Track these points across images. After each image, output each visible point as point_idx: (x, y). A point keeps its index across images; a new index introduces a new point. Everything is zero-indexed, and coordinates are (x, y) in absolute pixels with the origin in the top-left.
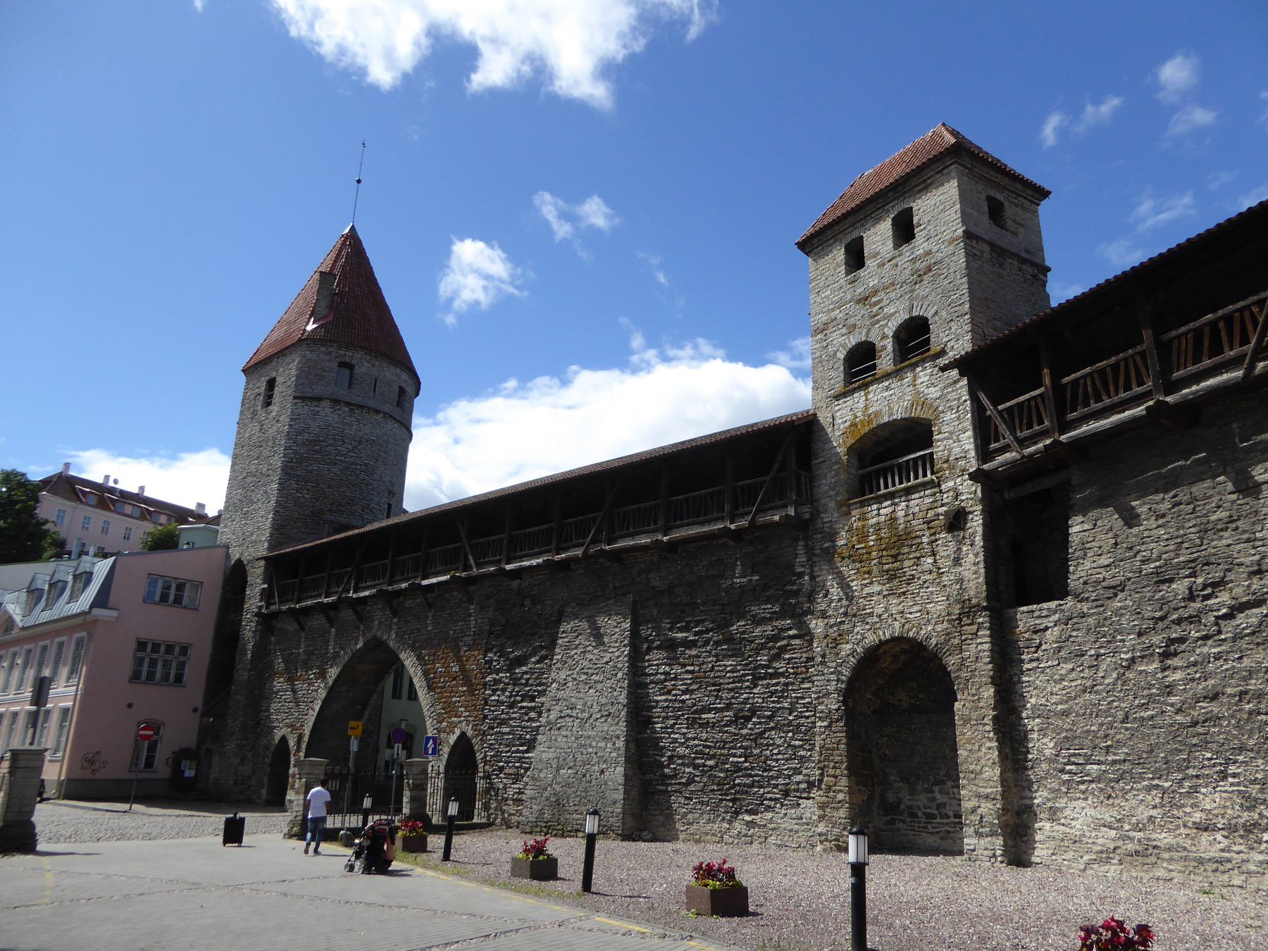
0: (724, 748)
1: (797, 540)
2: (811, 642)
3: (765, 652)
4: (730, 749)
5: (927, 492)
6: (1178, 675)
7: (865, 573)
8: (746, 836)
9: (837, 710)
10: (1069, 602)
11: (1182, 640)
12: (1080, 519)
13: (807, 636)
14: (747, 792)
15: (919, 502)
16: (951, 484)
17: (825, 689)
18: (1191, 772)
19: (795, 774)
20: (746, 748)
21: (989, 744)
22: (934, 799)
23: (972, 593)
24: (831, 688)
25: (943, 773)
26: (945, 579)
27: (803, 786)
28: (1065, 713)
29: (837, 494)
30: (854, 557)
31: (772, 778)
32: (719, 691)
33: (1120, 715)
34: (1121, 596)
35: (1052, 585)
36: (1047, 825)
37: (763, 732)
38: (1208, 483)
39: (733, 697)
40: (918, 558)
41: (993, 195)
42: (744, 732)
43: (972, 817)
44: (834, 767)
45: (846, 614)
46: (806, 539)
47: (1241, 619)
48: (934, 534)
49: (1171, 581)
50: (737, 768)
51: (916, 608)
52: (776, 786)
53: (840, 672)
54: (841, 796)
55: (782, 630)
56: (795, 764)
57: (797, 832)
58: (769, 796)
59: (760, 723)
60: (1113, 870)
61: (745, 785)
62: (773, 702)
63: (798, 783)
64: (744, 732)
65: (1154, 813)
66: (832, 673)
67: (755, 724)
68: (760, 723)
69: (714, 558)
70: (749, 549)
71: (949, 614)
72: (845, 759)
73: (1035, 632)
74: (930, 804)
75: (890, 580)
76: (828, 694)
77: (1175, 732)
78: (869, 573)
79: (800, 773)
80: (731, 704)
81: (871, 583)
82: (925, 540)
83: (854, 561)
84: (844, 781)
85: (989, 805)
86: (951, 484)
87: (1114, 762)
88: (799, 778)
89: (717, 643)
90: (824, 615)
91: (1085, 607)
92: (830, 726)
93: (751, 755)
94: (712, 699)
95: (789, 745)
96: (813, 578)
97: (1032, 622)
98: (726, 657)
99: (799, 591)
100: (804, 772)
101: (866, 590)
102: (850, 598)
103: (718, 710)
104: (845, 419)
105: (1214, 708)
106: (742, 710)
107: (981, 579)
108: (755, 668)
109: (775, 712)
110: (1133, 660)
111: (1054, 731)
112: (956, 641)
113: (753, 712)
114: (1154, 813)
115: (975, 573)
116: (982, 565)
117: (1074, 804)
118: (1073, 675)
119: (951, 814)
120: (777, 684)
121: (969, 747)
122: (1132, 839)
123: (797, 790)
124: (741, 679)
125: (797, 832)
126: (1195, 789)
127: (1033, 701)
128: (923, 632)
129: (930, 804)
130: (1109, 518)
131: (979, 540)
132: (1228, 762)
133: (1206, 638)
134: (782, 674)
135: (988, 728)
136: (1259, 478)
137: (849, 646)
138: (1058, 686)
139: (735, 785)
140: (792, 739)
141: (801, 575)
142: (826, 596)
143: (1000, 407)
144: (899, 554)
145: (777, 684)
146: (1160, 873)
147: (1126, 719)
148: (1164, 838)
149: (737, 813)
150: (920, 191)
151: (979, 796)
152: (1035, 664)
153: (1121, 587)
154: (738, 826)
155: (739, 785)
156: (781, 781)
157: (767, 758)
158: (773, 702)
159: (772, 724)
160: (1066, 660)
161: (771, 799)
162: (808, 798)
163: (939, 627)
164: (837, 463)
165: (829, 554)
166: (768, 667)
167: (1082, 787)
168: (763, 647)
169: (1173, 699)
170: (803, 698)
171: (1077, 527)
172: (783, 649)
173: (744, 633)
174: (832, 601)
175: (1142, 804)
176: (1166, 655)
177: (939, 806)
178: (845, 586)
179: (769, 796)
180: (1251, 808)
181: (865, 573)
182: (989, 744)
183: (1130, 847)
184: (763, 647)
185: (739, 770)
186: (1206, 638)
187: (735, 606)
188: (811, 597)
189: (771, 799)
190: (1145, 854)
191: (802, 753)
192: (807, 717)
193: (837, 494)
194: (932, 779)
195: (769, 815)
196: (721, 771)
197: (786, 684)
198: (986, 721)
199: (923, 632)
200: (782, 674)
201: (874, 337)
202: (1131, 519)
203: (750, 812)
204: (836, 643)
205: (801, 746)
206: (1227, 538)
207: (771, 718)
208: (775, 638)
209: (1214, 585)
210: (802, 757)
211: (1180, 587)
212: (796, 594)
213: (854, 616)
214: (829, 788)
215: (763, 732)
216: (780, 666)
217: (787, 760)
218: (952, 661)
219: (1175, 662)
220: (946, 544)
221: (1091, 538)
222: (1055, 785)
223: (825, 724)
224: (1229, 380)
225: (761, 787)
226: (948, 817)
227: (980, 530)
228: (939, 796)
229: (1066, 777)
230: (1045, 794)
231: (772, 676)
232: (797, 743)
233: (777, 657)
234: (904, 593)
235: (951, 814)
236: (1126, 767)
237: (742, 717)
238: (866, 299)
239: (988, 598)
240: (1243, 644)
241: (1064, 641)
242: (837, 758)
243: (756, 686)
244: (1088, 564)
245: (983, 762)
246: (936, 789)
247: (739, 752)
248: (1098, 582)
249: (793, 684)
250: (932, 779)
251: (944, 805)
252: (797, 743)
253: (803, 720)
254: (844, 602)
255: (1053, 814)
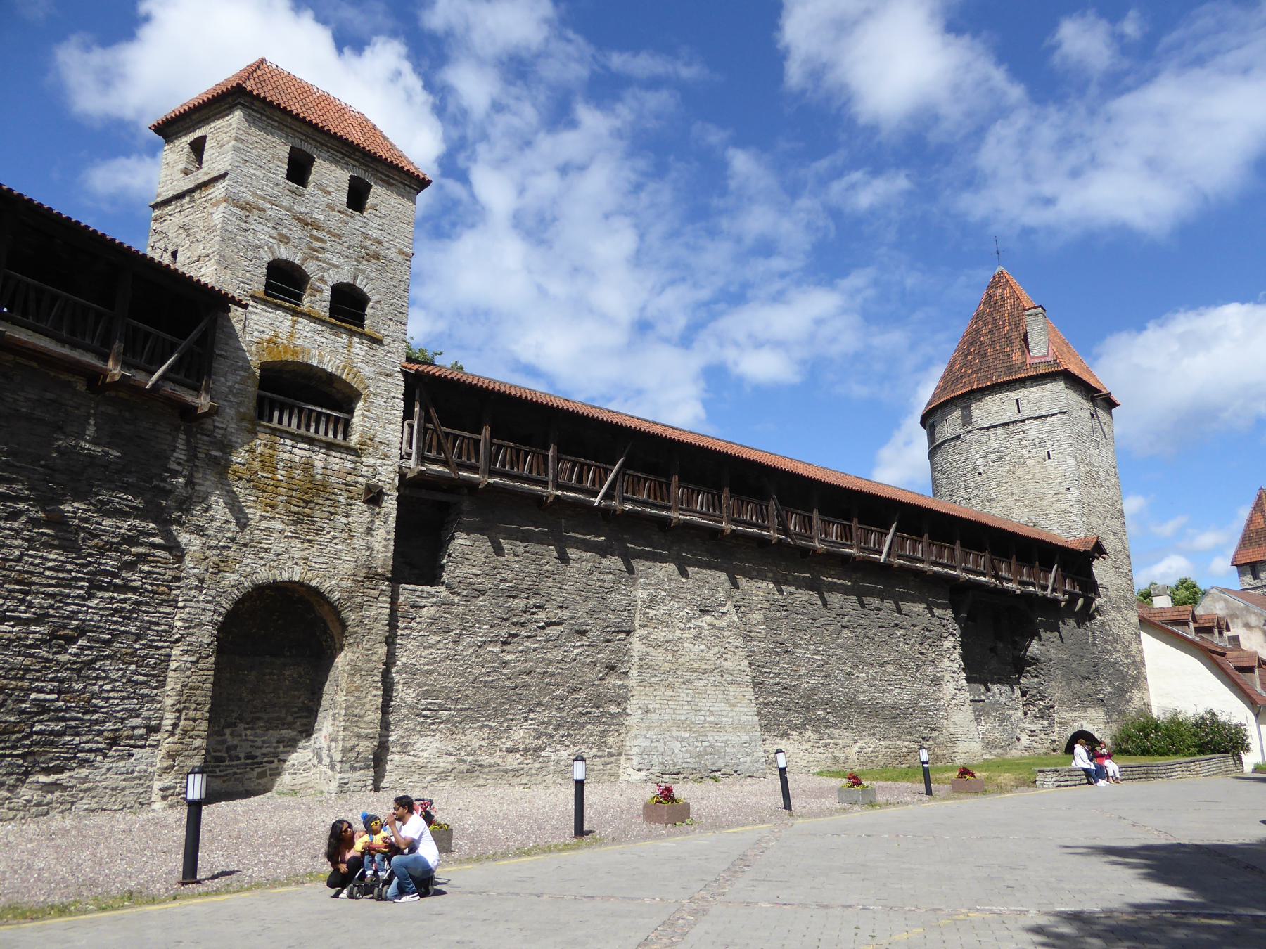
0: (22, 678)
1: (177, 429)
2: (180, 559)
3: (115, 555)
4: (33, 680)
5: (349, 457)
6: (510, 657)
7: (268, 505)
8: (39, 805)
9: (209, 645)
10: (442, 590)
11: (515, 636)
12: (464, 535)
13: (177, 552)
14: (52, 743)
15: (336, 461)
16: (372, 461)
17: (194, 618)
18: (510, 717)
19: (130, 716)
20: (61, 681)
21: (374, 692)
22: (224, 742)
23: (380, 563)
24: (206, 618)
25: (235, 715)
26: (356, 543)
27: (142, 731)
28: (430, 672)
29: (240, 404)
30: (255, 484)
31: (97, 722)
32: (27, 593)
33: (471, 678)
34: (481, 598)
35: (431, 576)
36: (397, 757)
37: (94, 661)
38: (544, 547)
39: (52, 607)
40: (332, 514)
41: (298, 146)
42: (64, 658)
43: (350, 755)
44: (196, 710)
45: (233, 540)
46: (188, 433)
47: (548, 630)
48: (351, 498)
49: (514, 597)
50: (42, 708)
51: (321, 560)
52: (100, 733)
53: (218, 604)
54: (198, 742)
55: (141, 533)
56: (133, 704)
57: (123, 790)
58: (88, 746)
59: (90, 648)
60: (448, 784)
61: (52, 733)
62: (116, 623)
63: (133, 728)
64: (64, 658)
65: (483, 743)
66: (208, 602)
67: (82, 648)
68: (90, 648)
69: (50, 396)
70: (110, 410)
71: (354, 575)
72: (208, 700)
73: (412, 607)
74: (219, 747)
75: (296, 523)
76: (201, 624)
77: (504, 692)
78: (273, 507)
79: (138, 716)
80: (47, 615)
81: (273, 518)
82: (342, 499)
83: (254, 487)
84: (204, 725)
85: (368, 743)
86: (372, 461)
87: (461, 709)
88: (136, 722)
89: (35, 522)
90: (200, 531)
91: (456, 599)
92: (197, 662)
93: (69, 690)
94: (11, 604)
95: (129, 681)
96: (190, 482)
97: (413, 599)
98: (49, 546)
99: (170, 492)
100: (145, 714)
101: (265, 524)
102: (243, 523)
103: (19, 621)
104: (261, 330)
105: (528, 678)
106: (64, 627)
107: (390, 554)
108: (95, 574)
109: (116, 635)
110: (485, 642)
111: (418, 685)
112: (359, 600)
113: (81, 631)
114: (483, 743)
115: (385, 547)
116: (392, 543)
117: (423, 739)
118: (440, 645)
119: (242, 755)
120: (125, 600)
121: (357, 694)
122: (465, 761)
123: (130, 738)
124: (69, 583)
125: (123, 790)
126: (509, 728)
127: (404, 660)
128: (327, 584)
129: (219, 747)
130: (484, 544)
131: (392, 520)
132: (531, 711)
133: (529, 637)
134: (134, 590)
135: (376, 679)
136: (572, 556)
137: (234, 577)
138: (426, 652)
139: (32, 734)
140: (134, 673)
141: (175, 474)
142: (206, 511)
143: (495, 441)
144: (312, 502)
145: (125, 600)
146: (481, 782)
147: (474, 681)
148: (486, 759)
149: (27, 774)
150: (382, 180)
151: (359, 736)
152: (408, 632)
153: (482, 592)
154: (26, 793)
155: (37, 733)
156: (109, 726)
157: (93, 696)
158: (116, 623)
159: (108, 652)
160: (435, 633)
161: (90, 751)
162: (143, 747)
163: (343, 584)
164: (243, 368)
165: (221, 468)
166: (115, 575)
167: (433, 727)
168: (112, 547)
169: (506, 671)
170: (157, 624)
171: (461, 541)
172: (141, 558)
173: (86, 520)
174: (214, 519)
175: (474, 738)
176: (504, 643)
177: (229, 749)
178: (235, 506)
179: (88, 746)
180: (538, 738)
181: (268, 505)
182: (374, 692)
183: (463, 767)
184: (112, 547)
185: (45, 711)
186: (529, 637)
187: (81, 478)
188: (185, 505)
189: (90, 751)
190: (474, 770)
191: (146, 691)
192: (158, 648)
193: (240, 404)
194: (222, 721)
195: (83, 772)
196: (11, 712)
197: (138, 603)
198: (375, 672)
199: (327, 584)
200: (134, 590)
201: (311, 268)
202: (499, 551)
203: (47, 771)
204: (218, 569)
205: (145, 683)
206: (549, 583)
207: (108, 643)
208: (131, 541)
209: (538, 607)
210: (144, 696)
211: (519, 603)
212: (167, 493)
213: (245, 545)
214: (185, 733)
215: (94, 661)
216: (134, 578)
217: (123, 698)
218: (351, 617)
219: (508, 648)
220: (360, 514)
221: (466, 552)
222: (411, 726)
223: (193, 658)
224: (92, 365)
225: (78, 734)
226: (239, 759)
227: (394, 513)
228: (228, 738)
229: (421, 719)
230: (400, 733)
231: (118, 589)
232: (141, 678)
233: (130, 566)
234: (310, 541)
235: (242, 755)
236: (468, 713)
237: (60, 638)
238: (307, 225)
239: (393, 572)
240: (548, 645)
241: (434, 620)
242: (200, 700)
243: (91, 596)
244: (464, 570)
245: (368, 707)
246: (228, 731)
247: (49, 686)
248: (470, 584)
249: (147, 604)
250: (222, 721)
251: (235, 747)
252: (141, 678)
253: (153, 651)
254: (232, 526)
255: (404, 749)
